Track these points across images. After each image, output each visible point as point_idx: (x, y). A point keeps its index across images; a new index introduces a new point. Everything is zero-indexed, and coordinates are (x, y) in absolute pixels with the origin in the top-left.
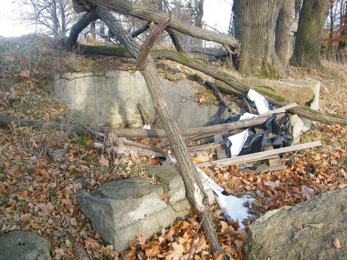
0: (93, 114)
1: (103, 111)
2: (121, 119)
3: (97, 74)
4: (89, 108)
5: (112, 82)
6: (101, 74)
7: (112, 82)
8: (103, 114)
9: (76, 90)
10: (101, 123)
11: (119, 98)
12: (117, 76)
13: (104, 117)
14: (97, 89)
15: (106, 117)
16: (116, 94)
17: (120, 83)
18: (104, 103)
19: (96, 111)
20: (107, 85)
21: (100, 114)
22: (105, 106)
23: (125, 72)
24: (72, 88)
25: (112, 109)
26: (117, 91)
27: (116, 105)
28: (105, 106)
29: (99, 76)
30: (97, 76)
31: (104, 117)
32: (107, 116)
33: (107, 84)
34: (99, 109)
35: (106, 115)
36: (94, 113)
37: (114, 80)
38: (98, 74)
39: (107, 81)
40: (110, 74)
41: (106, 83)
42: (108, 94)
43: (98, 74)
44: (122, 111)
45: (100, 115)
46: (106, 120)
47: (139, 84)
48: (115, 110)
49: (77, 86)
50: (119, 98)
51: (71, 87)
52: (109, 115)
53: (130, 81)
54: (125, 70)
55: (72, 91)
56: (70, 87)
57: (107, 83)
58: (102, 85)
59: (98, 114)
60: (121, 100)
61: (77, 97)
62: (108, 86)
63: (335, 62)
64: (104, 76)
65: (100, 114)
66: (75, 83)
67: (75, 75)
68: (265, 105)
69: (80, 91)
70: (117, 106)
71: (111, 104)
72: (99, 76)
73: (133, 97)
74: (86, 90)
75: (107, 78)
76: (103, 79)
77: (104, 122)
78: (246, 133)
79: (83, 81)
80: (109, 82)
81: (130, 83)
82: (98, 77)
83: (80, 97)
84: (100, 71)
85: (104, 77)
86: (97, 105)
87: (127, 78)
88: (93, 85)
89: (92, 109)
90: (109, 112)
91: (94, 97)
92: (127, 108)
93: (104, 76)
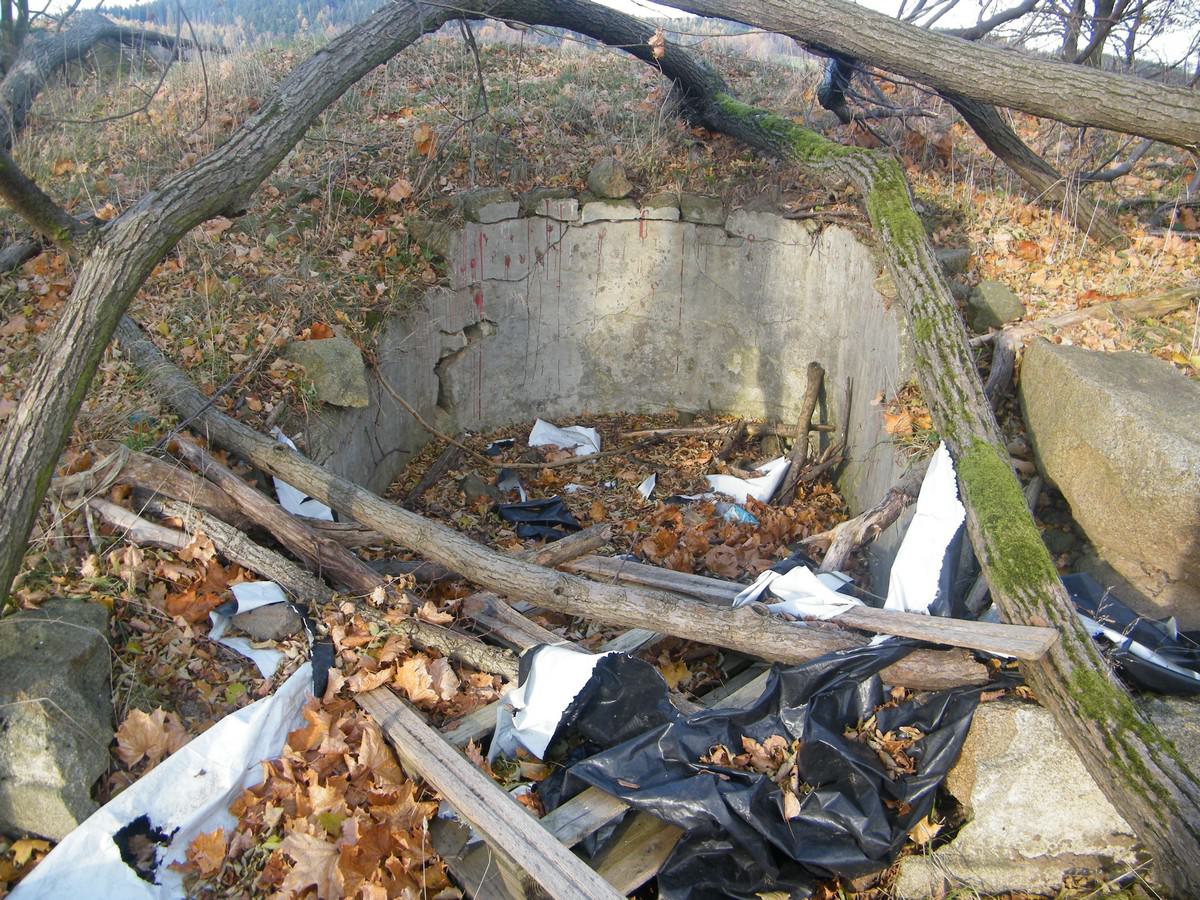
0: (666, 359)
1: (705, 359)
2: (763, 406)
3: (694, 215)
4: (649, 334)
5: (748, 257)
6: (711, 217)
7: (748, 257)
8: (700, 370)
9: (600, 262)
10: (690, 400)
11: (768, 326)
12: (765, 236)
13: (704, 381)
14: (690, 273)
15: (712, 384)
16: (754, 301)
17: (772, 264)
18: (708, 329)
19: (679, 353)
20: (727, 265)
21: (691, 365)
22: (715, 340)
23: (794, 225)
24: (584, 256)
25: (737, 358)
26: (760, 292)
27: (750, 348)
28: (715, 340)
29: (706, 225)
30: (698, 224)
31: (704, 381)
32: (716, 380)
33: (730, 261)
34: (688, 349)
35: (711, 376)
36: (668, 356)
37: (754, 252)
38: (697, 217)
39: (729, 249)
40: (745, 222)
41: (725, 256)
42: (728, 298)
43: (697, 217)
44: (770, 379)
45: (690, 369)
46: (710, 394)
47: (830, 283)
48: (745, 364)
49: (607, 249)
50: (765, 324)
51: (582, 249)
52: (723, 380)
53: (806, 264)
54: (793, 216)
55: (582, 263)
56: (576, 248)
57: (728, 255)
58: (712, 261)
59: (682, 366)
60: (770, 335)
61: (602, 289)
62: (732, 267)
63: (1099, 842)
64: (722, 226)
65: (691, 365)
66: (601, 237)
67: (597, 209)
68: (558, 718)
69: (623, 268)
70: (756, 351)
71: (735, 341)
72: (706, 225)
73: (808, 331)
74: (647, 269)
75: (730, 235)
76: (717, 238)
77: (701, 399)
78: (728, 796)
79: (637, 236)
80: (737, 255)
81: (804, 273)
82: (699, 230)
83: (617, 291)
84: (711, 207)
85: (719, 232)
86: (683, 331)
87: (799, 251)
88: (675, 256)
89: (662, 341)
90: (723, 367)
91: (676, 298)
92: (785, 370)
93: (722, 226)
